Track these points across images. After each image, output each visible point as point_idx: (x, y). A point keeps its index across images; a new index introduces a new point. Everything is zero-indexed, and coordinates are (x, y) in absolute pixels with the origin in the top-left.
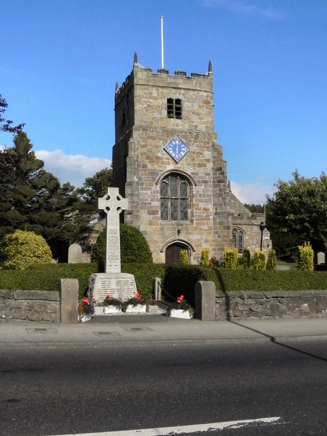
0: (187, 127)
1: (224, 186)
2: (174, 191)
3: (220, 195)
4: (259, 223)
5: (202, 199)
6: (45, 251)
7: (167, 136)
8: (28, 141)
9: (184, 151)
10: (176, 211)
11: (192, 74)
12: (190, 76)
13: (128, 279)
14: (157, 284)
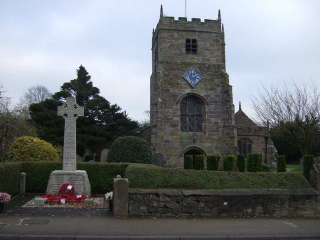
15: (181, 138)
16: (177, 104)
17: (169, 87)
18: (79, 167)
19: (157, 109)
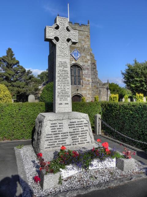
0: (80, 46)
1: (96, 70)
2: (75, 73)
3: (94, 74)
4: (106, 87)
5: (87, 77)
6: (5, 95)
7: (72, 49)
8: (12, 52)
9: (79, 56)
10: (76, 81)
11: (82, 25)
12: (81, 25)
13: (82, 120)
14: (98, 119)
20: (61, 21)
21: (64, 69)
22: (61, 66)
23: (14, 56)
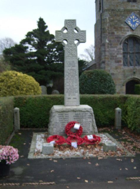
15: (124, 71)
16: (120, 44)
17: (114, 30)
18: (83, 101)
19: (105, 49)
20: (69, 24)
21: (72, 69)
22: (69, 66)
23: (26, 82)
